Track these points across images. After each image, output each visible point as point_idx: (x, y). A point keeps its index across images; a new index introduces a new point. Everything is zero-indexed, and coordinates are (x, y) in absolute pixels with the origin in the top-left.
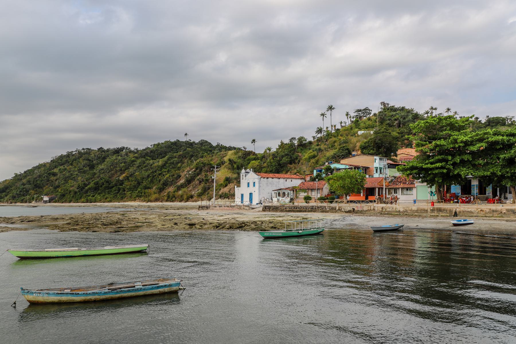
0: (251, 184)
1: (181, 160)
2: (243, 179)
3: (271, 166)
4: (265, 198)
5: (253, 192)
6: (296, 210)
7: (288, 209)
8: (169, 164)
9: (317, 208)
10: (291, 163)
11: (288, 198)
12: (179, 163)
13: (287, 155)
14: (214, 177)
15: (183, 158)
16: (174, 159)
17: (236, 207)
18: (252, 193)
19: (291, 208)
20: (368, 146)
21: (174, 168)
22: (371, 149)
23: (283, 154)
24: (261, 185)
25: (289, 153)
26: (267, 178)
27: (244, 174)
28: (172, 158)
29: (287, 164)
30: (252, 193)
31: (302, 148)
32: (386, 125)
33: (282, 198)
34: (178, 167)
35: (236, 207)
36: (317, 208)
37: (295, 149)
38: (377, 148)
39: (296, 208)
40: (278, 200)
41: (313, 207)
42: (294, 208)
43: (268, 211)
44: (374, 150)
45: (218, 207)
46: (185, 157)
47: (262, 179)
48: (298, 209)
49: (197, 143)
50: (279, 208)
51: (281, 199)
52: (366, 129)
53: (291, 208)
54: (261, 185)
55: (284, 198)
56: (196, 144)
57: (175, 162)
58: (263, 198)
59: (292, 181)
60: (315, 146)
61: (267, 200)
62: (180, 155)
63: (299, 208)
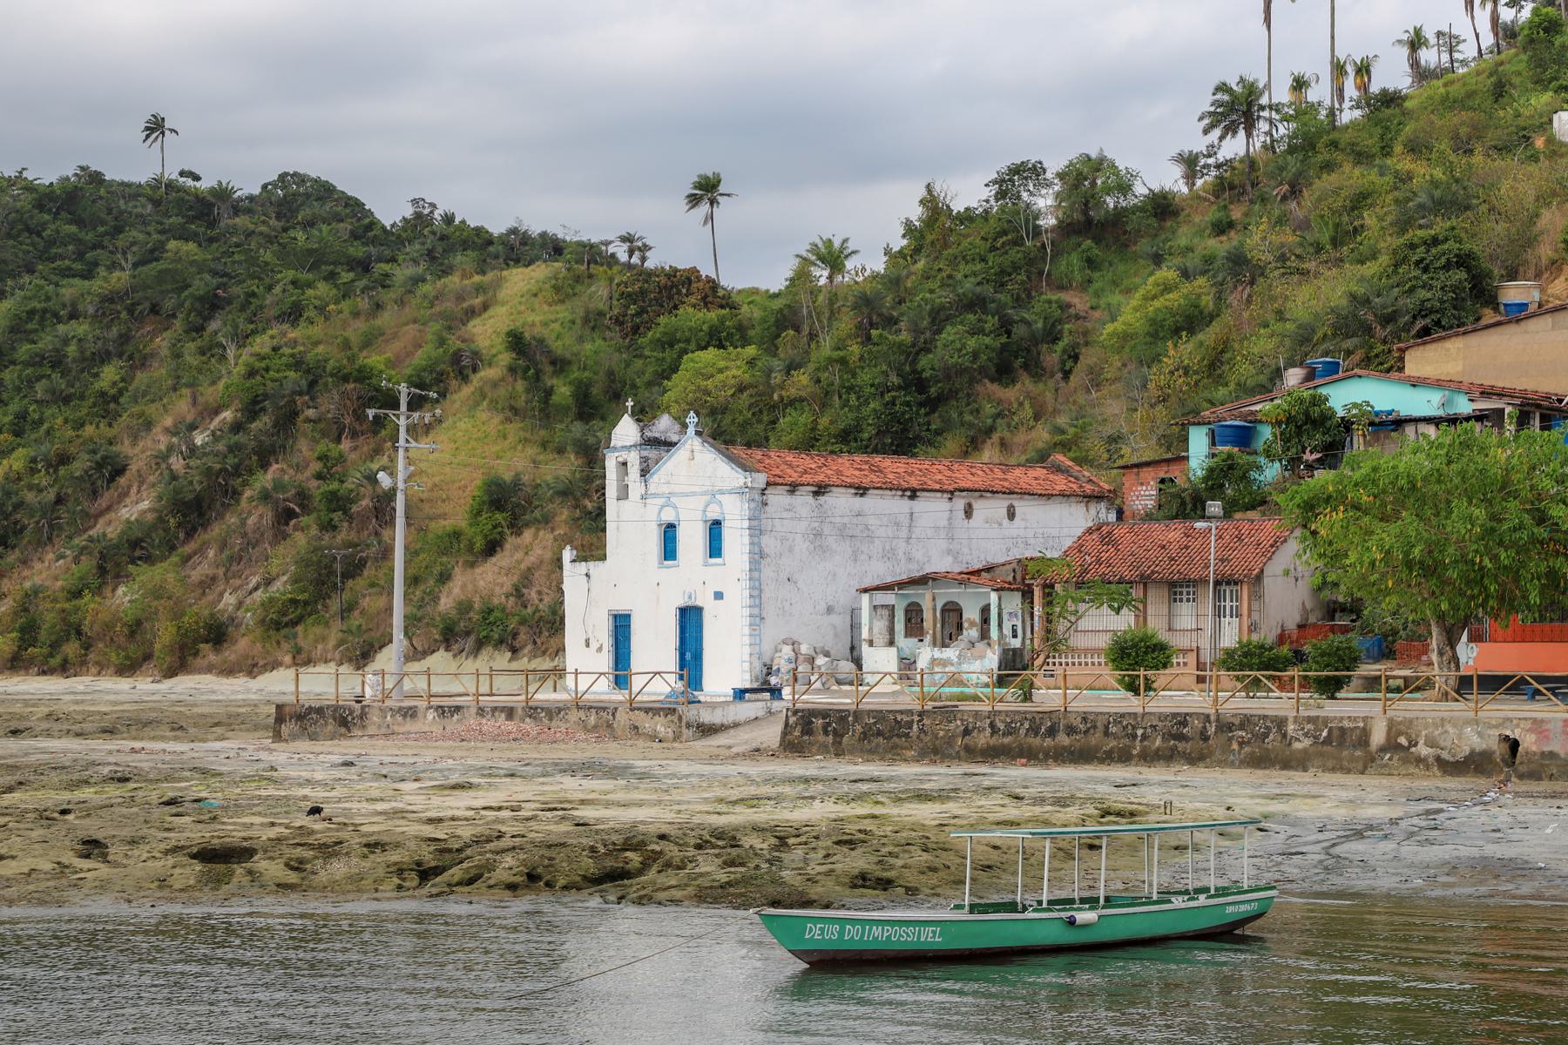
0: (692, 539)
1: (125, 338)
2: (623, 494)
3: (850, 389)
4: (804, 649)
5: (704, 600)
6: (1048, 742)
7: (983, 739)
8: (27, 364)
9: (1212, 730)
10: (1003, 372)
11: (980, 646)
12: (104, 357)
13: (975, 304)
14: (392, 474)
15: (140, 319)
16: (61, 328)
17: (574, 716)
18: (698, 610)
19: (1010, 731)
21: (67, 400)
24: (768, 543)
25: (988, 290)
26: (820, 490)
27: (633, 459)
28: (47, 316)
29: (972, 381)
30: (698, 610)
33: (938, 653)
34: (103, 394)
35: (574, 716)
36: (1212, 730)
39: (1052, 732)
41: (1184, 723)
42: (1034, 730)
43: (824, 749)
45: (431, 715)
46: (155, 310)
47: (778, 498)
48: (1063, 739)
49: (251, 198)
50: (910, 725)
51: (925, 654)
53: (1010, 731)
55: (950, 653)
56: (237, 208)
57: (72, 349)
59: (1011, 515)
61: (821, 661)
62: (110, 299)
63: (1071, 730)
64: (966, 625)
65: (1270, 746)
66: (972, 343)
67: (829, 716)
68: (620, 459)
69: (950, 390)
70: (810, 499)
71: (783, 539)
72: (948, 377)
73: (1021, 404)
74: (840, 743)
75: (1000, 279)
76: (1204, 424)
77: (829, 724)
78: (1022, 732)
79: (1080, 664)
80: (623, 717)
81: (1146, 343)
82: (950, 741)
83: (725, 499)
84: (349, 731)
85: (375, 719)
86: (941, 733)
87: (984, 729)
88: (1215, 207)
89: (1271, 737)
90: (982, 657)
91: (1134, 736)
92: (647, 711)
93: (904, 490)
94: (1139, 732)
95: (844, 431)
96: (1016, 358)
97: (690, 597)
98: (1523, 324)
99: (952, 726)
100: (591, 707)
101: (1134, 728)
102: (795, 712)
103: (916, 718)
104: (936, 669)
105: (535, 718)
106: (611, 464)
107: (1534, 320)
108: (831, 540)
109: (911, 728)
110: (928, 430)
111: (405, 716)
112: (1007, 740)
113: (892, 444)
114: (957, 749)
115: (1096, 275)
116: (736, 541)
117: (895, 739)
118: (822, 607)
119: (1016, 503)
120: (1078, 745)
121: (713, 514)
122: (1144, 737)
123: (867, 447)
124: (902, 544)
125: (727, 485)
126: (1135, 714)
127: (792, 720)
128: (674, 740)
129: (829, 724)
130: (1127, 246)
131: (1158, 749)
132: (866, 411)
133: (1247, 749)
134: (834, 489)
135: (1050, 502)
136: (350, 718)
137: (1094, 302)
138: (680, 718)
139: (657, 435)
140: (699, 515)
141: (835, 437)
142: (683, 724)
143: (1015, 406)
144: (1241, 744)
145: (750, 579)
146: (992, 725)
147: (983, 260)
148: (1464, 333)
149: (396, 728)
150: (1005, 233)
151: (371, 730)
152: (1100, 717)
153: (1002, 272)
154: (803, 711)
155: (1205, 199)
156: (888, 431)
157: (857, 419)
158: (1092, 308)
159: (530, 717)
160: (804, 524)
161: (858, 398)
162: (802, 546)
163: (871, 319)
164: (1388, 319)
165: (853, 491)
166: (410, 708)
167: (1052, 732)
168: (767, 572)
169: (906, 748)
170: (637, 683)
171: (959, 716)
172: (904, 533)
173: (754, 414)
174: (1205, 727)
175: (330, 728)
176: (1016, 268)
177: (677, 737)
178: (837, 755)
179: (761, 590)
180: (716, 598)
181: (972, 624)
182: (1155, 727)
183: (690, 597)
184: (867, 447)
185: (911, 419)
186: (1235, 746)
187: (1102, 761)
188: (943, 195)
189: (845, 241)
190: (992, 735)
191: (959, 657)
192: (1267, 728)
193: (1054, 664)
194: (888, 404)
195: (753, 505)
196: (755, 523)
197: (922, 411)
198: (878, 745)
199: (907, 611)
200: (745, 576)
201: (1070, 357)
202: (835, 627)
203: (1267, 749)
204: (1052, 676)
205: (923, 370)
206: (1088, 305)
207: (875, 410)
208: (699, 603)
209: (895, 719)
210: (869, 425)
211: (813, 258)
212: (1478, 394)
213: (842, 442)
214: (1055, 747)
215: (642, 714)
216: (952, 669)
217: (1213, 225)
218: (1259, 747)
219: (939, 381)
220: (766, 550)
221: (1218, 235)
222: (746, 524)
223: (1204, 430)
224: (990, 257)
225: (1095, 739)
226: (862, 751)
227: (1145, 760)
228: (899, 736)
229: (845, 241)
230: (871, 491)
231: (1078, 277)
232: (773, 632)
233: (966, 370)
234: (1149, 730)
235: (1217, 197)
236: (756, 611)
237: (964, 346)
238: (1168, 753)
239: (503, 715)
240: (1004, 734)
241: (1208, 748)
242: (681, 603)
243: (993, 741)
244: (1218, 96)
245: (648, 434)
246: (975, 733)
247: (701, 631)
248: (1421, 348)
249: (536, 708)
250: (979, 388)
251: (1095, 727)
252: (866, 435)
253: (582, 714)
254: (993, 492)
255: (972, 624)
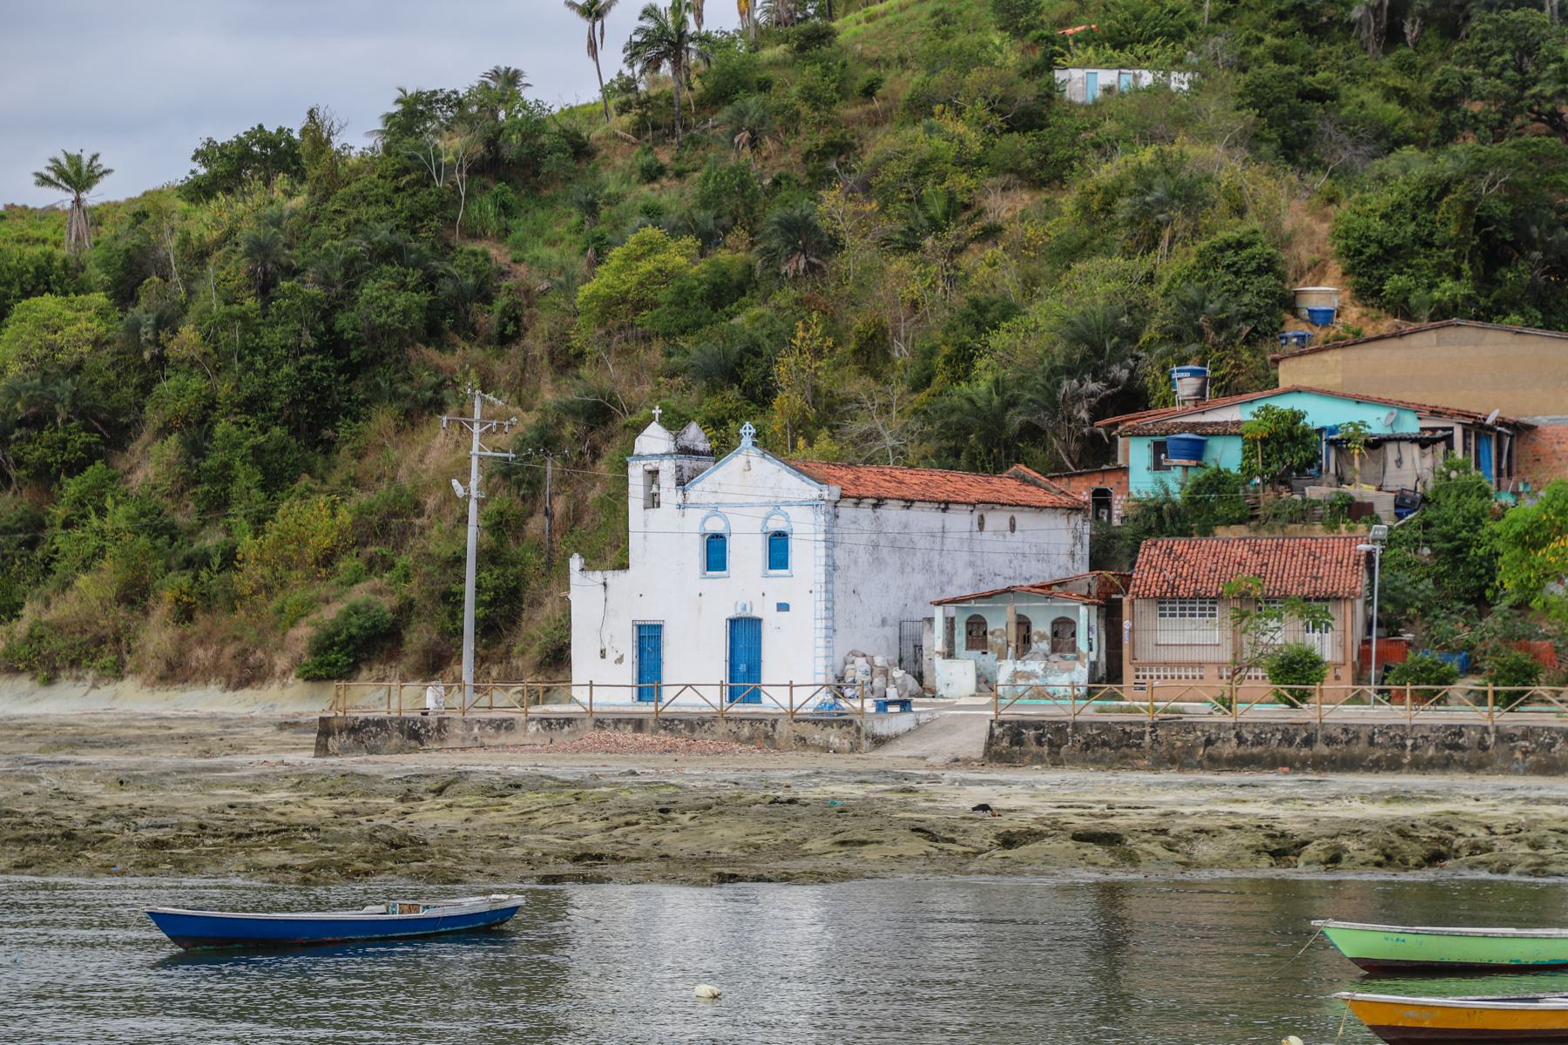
0: (747, 551)
2: (653, 501)
3: (254, 351)
4: (879, 661)
5: (764, 610)
6: (1304, 751)
7: (1229, 749)
9: (1491, 740)
10: (433, 334)
13: (390, 254)
14: (464, 482)
17: (721, 728)
18: (756, 623)
19: (1258, 742)
20: (1416, 238)
22: (1442, 268)
23: (358, 245)
25: (400, 237)
26: (879, 503)
27: (667, 469)
29: (402, 345)
30: (756, 623)
31: (511, 196)
32: (1281, 16)
33: (1020, 666)
35: (721, 728)
36: (1491, 740)
37: (446, 204)
38: (1480, 263)
39: (1309, 742)
40: (985, 682)
41: (1460, 734)
42: (1288, 740)
43: (1039, 759)
44: (1457, 275)
45: (533, 727)
47: (846, 511)
48: (1321, 749)
50: (1141, 736)
51: (1006, 670)
52: (1119, 46)
53: (1258, 742)
54: (839, 553)
58: (861, 662)
59: (1013, 528)
60: (626, 179)
63: (1330, 740)
64: (1035, 638)
65: (1557, 755)
66: (401, 300)
67: (1043, 727)
68: (649, 468)
69: (376, 354)
70: (869, 511)
71: (851, 551)
72: (373, 339)
73: (466, 374)
74: (1058, 753)
75: (414, 221)
76: (1144, 435)
77: (1043, 735)
78: (1274, 742)
79: (1173, 677)
80: (784, 728)
81: (671, 314)
82: (1190, 750)
83: (795, 513)
84: (422, 744)
85: (457, 731)
86: (1179, 744)
87: (1229, 740)
88: (638, 150)
89: (1558, 746)
90: (1070, 670)
91: (1404, 747)
92: (816, 723)
93: (940, 503)
94: (1409, 742)
95: (247, 398)
96: (443, 317)
97: (744, 608)
98: (1406, 339)
99: (1191, 737)
100: (741, 720)
101: (1402, 738)
102: (1001, 724)
103: (1148, 729)
104: (1019, 682)
105: (671, 730)
106: (636, 473)
107: (1418, 336)
108: (885, 550)
109: (1142, 738)
110: (349, 400)
111: (498, 728)
112: (1256, 750)
113: (307, 415)
114: (1198, 758)
115: (513, 223)
116: (807, 554)
117: (1125, 749)
118: (878, 620)
119: (1015, 515)
120: (1339, 754)
121: (777, 525)
122: (1415, 747)
123: (276, 418)
124: (937, 557)
125: (795, 496)
126: (1403, 726)
127: (998, 731)
128: (852, 751)
129: (1043, 735)
130: (538, 190)
131: (1432, 758)
132: (276, 377)
133: (1532, 758)
134: (955, 506)
135: (1041, 515)
136: (423, 731)
137: (517, 254)
138: (858, 730)
139: (687, 443)
140: (757, 525)
141: (238, 405)
142: (863, 735)
143: (460, 375)
144: (1525, 753)
145: (826, 591)
146: (1238, 736)
147: (389, 202)
148: (1343, 346)
149: (486, 741)
150: (407, 171)
151: (451, 743)
152: (1363, 729)
153: (412, 218)
154: (1010, 722)
155: (624, 140)
156: (303, 401)
157: (266, 386)
158: (515, 261)
159: (665, 729)
160: (865, 537)
161: (265, 361)
162: (864, 557)
163: (265, 269)
164: (1221, 326)
165: (902, 503)
166: (505, 720)
167: (1309, 742)
168: (838, 584)
169: (1138, 758)
170: (668, 694)
171: (1199, 727)
172: (937, 546)
173: (118, 376)
174: (1483, 738)
175: (395, 741)
176: (428, 212)
177: (854, 749)
178: (1054, 764)
179: (834, 603)
180: (778, 610)
181: (1042, 637)
182: (1426, 737)
183: (744, 608)
184: (276, 418)
185: (329, 386)
186: (1518, 755)
187: (1368, 769)
188: (327, 123)
189: (95, 157)
190: (1239, 745)
191: (1045, 670)
192: (1552, 738)
193: (1144, 677)
194: (303, 367)
195: (828, 518)
196: (829, 536)
197: (342, 378)
198: (1104, 755)
199: (968, 623)
200: (819, 588)
201: (510, 319)
202: (887, 639)
203: (1554, 758)
204: (1142, 689)
205: (343, 332)
206: (509, 257)
207: (288, 375)
208: (756, 614)
209: (1124, 730)
210: (281, 392)
211: (52, 175)
212: (1427, 413)
213: (246, 412)
214: (1313, 756)
215: (810, 726)
216: (1037, 682)
217: (643, 169)
218: (1545, 756)
219: (363, 344)
220: (838, 562)
221: (649, 182)
222: (822, 537)
223: (1146, 441)
224: (398, 200)
225: (1359, 748)
226: (1084, 760)
227: (1417, 768)
228: (1128, 746)
229: (95, 157)
230: (917, 504)
231: (494, 225)
232: (843, 646)
233: (396, 329)
234: (1420, 741)
235: (638, 137)
236: (830, 623)
237: (392, 304)
238: (1443, 762)
239: (630, 727)
240: (1252, 745)
241: (1488, 757)
242: (732, 614)
243: (1241, 751)
244: (644, 24)
245: (681, 443)
246: (1219, 744)
247: (760, 644)
248: (1297, 359)
249: (673, 720)
250: (411, 352)
251: (1358, 737)
252: (277, 405)
253: (732, 726)
254: (1003, 504)
255: (1042, 637)
